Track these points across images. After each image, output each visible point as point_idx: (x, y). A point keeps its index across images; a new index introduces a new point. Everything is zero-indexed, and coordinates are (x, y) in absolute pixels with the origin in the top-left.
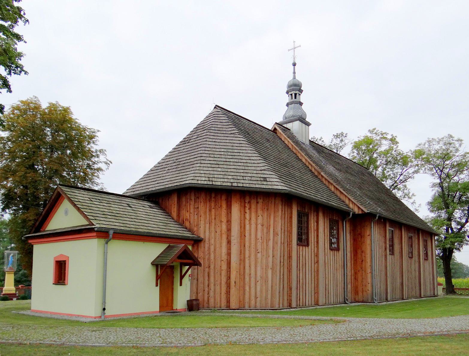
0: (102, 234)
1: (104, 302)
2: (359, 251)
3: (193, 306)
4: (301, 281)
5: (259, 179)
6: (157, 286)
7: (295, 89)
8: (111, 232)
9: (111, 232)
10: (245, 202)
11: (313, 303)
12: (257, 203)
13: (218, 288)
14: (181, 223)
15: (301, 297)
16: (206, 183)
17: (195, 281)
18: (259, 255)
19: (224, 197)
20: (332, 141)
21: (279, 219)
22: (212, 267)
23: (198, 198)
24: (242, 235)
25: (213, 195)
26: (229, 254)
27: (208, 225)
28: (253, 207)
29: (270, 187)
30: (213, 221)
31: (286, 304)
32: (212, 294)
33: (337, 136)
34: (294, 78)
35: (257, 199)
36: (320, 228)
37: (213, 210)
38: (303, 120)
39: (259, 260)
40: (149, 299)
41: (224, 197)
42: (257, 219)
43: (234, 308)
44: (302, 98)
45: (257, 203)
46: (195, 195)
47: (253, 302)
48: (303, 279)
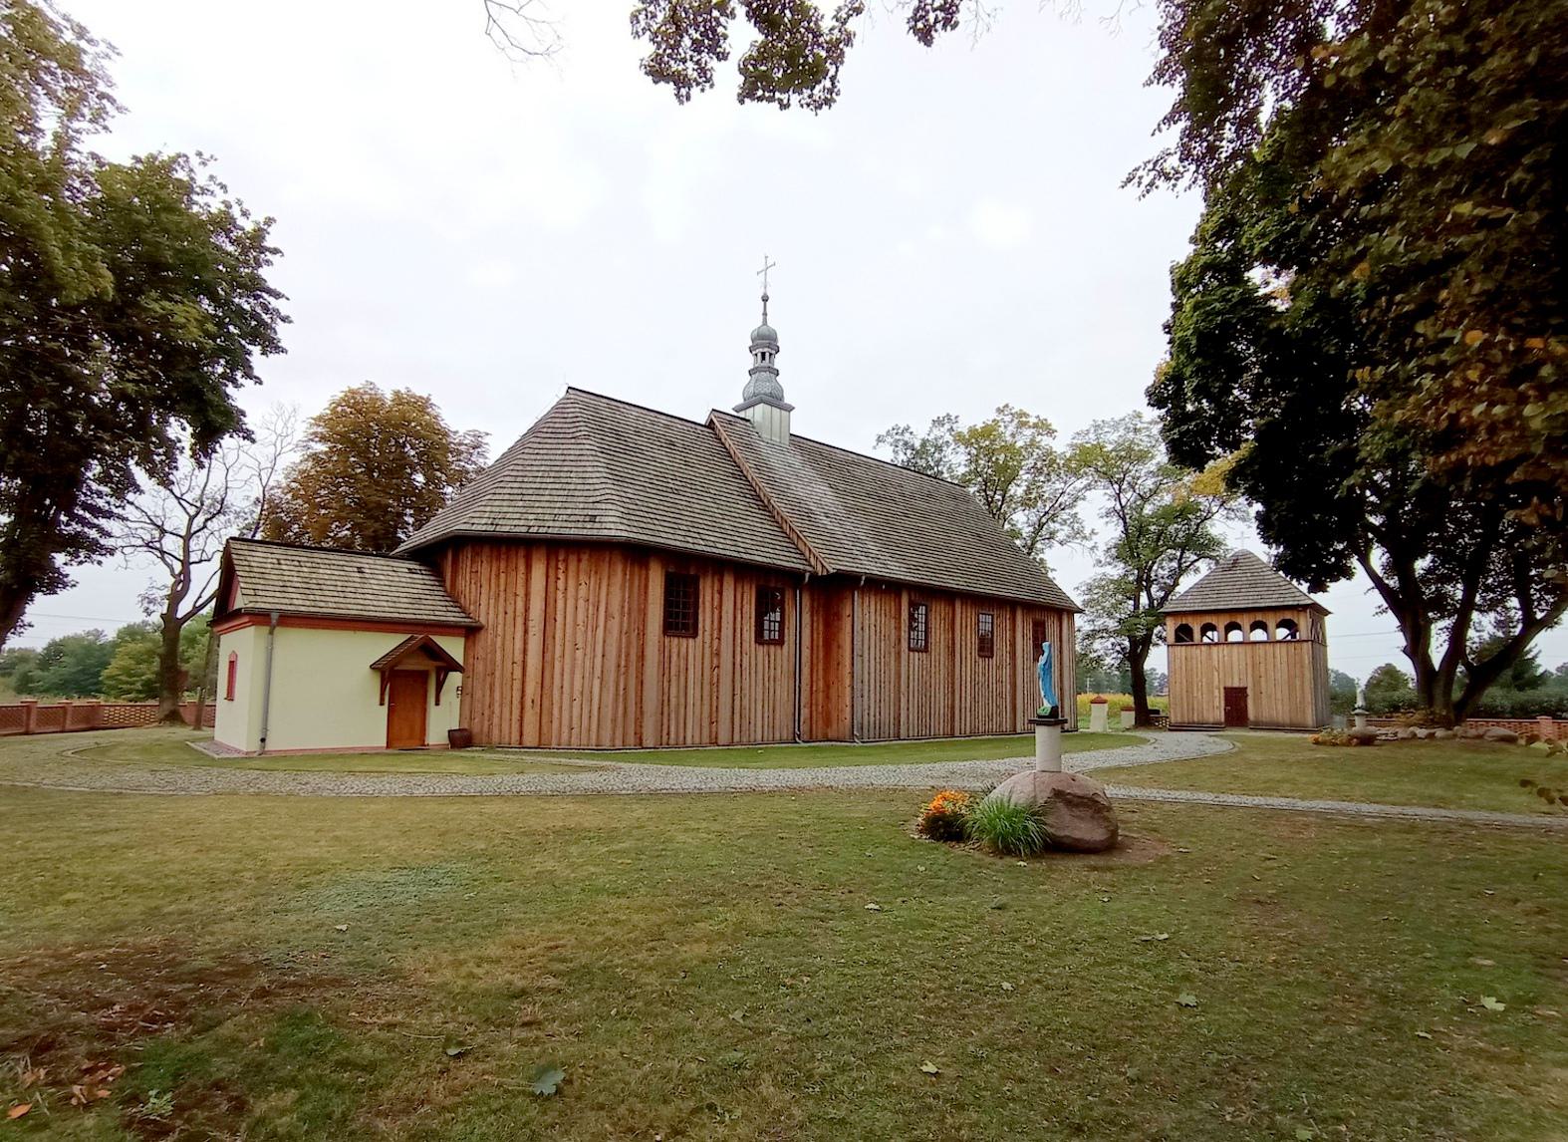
0: (260, 618)
1: (265, 729)
2: (834, 647)
3: (461, 740)
4: (673, 701)
5: (581, 518)
6: (382, 704)
7: (765, 345)
8: (275, 616)
9: (275, 616)
10: (557, 561)
11: (706, 740)
12: (579, 561)
13: (506, 710)
14: (454, 597)
15: (673, 729)
16: (484, 528)
17: (468, 698)
18: (579, 653)
19: (521, 553)
20: (931, 431)
21: (616, 589)
22: (497, 674)
23: (477, 554)
24: (548, 618)
25: (504, 549)
26: (525, 651)
27: (492, 601)
28: (572, 567)
29: (595, 532)
30: (502, 594)
31: (631, 739)
32: (496, 721)
33: (938, 422)
34: (765, 322)
35: (579, 555)
36: (725, 608)
37: (503, 575)
38: (775, 400)
39: (579, 662)
40: (370, 724)
41: (521, 553)
42: (577, 591)
43: (529, 745)
44: (779, 362)
45: (579, 561)
46: (473, 548)
47: (565, 736)
48: (678, 697)
